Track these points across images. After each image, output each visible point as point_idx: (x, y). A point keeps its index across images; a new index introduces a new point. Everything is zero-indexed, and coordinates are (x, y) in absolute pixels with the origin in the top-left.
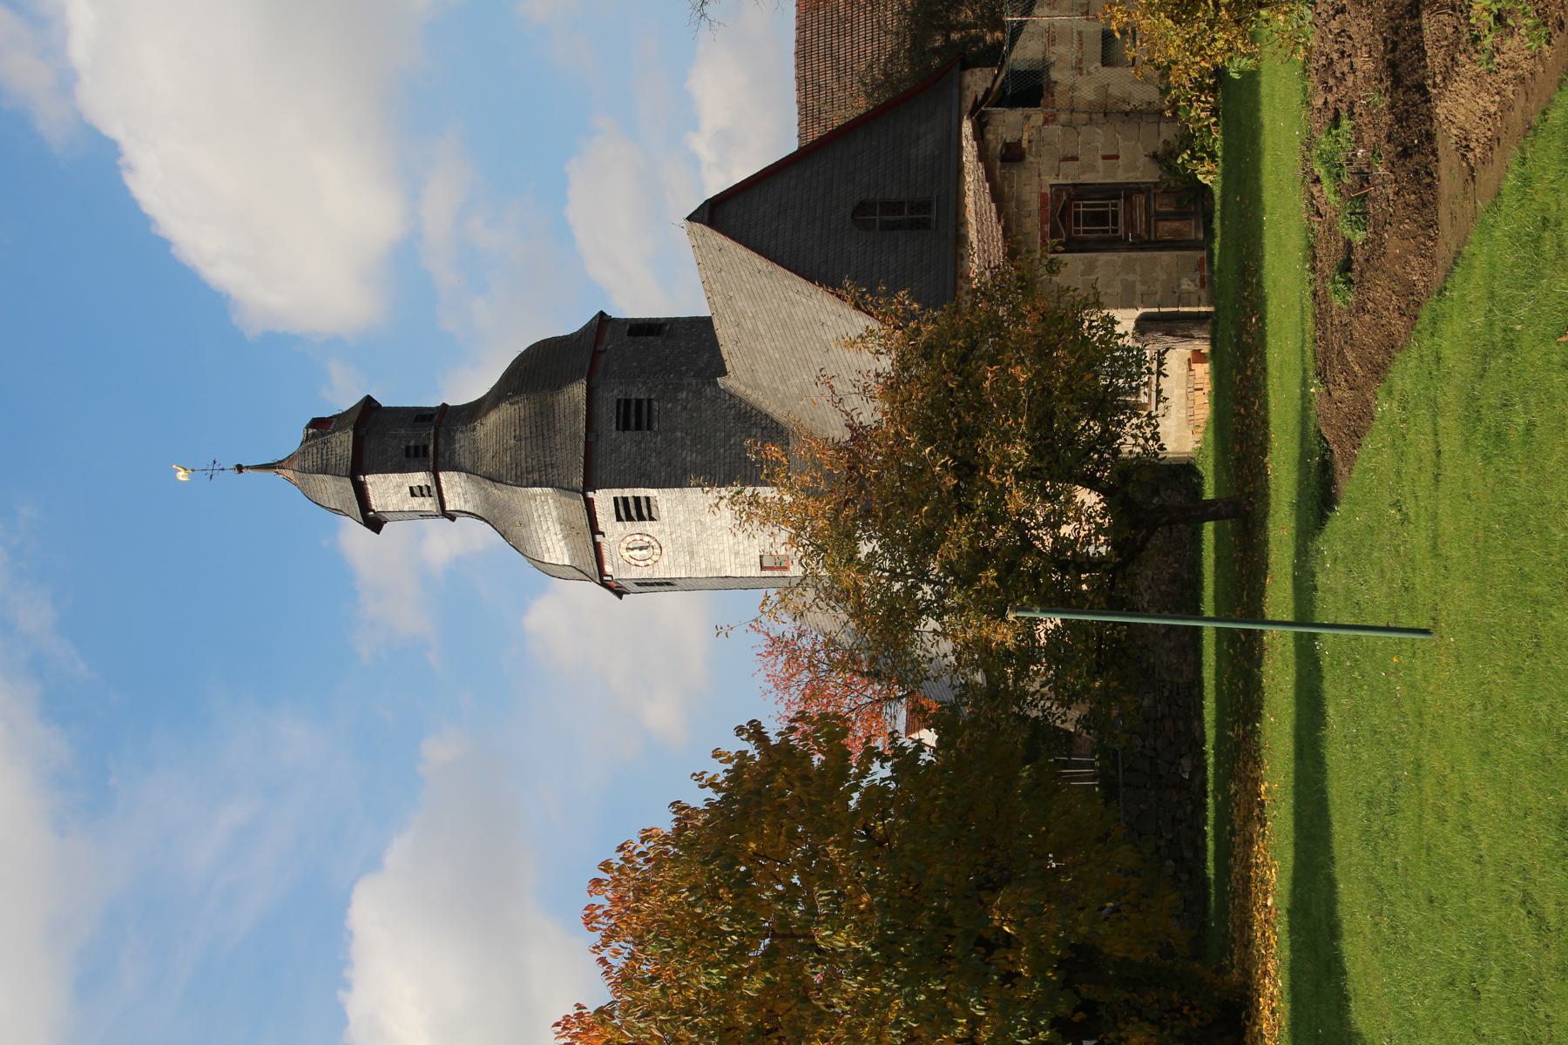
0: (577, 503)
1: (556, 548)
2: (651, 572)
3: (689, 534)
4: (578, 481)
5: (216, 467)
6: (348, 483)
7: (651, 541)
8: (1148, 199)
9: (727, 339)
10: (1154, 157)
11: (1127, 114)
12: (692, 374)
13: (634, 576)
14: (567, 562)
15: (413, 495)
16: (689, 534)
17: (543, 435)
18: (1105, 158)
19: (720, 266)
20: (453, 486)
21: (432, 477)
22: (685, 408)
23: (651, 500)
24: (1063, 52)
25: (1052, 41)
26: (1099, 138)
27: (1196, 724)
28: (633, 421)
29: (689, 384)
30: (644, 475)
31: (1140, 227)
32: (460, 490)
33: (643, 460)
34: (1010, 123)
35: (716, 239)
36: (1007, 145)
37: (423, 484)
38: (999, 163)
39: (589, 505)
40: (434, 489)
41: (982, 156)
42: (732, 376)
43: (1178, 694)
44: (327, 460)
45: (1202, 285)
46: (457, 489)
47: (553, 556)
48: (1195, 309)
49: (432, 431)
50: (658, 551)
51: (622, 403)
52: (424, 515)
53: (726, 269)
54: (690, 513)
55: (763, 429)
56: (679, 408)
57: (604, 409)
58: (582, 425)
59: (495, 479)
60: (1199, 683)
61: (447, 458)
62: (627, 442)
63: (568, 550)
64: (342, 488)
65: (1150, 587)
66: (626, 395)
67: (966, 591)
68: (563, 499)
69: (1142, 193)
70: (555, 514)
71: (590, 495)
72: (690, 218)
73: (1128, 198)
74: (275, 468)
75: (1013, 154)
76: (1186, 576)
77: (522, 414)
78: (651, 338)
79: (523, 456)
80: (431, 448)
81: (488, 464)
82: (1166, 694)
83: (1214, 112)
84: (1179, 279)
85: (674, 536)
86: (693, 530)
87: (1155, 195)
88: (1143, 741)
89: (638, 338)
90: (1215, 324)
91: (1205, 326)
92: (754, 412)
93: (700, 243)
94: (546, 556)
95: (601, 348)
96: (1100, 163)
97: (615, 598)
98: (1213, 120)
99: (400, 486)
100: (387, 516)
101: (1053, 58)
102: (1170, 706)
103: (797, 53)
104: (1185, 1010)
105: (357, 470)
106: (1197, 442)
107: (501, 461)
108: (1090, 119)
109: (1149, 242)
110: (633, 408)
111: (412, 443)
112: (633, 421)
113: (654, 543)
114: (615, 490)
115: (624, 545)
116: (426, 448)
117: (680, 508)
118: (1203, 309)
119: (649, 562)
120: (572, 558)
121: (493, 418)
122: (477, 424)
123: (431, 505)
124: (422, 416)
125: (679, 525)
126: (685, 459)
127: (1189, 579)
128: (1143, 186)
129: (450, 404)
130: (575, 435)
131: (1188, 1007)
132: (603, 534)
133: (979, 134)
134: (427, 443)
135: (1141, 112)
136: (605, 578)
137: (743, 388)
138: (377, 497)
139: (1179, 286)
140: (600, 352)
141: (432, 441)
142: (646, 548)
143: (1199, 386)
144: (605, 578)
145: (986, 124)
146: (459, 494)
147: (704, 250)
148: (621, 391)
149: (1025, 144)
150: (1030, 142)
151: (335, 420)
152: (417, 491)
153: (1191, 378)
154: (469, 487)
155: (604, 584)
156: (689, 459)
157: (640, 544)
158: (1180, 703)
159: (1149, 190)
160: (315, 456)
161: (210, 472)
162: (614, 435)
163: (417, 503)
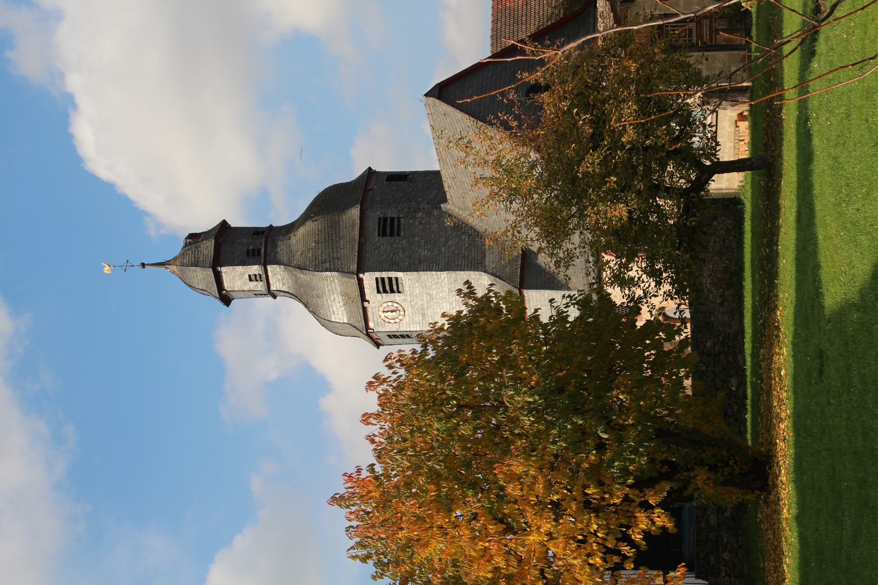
1: (339, 313)
2: (397, 327)
3: (422, 302)
4: (354, 267)
5: (128, 264)
6: (210, 272)
7: (399, 306)
9: (448, 176)
12: (425, 202)
13: (387, 330)
14: (346, 321)
15: (251, 280)
16: (422, 302)
17: (332, 240)
19: (444, 126)
20: (275, 274)
21: (263, 268)
22: (421, 223)
23: (399, 281)
27: (740, 357)
28: (388, 231)
29: (423, 208)
30: (395, 263)
31: (706, 38)
32: (280, 277)
33: (394, 254)
35: (443, 107)
37: (257, 273)
39: (360, 282)
40: (264, 276)
42: (450, 203)
43: (728, 339)
44: (198, 258)
46: (278, 276)
47: (337, 317)
49: (264, 240)
50: (402, 313)
51: (382, 219)
52: (258, 294)
53: (448, 127)
54: (423, 288)
55: (469, 236)
56: (417, 223)
57: (371, 223)
58: (357, 232)
59: (301, 268)
60: (742, 331)
61: (272, 257)
62: (385, 244)
63: (347, 313)
64: (207, 275)
65: (711, 275)
66: (384, 215)
68: (346, 279)
69: (708, 18)
70: (338, 289)
71: (361, 275)
72: (426, 95)
74: (165, 265)
76: (734, 268)
77: (320, 228)
78: (400, 182)
79: (320, 253)
80: (263, 251)
81: (298, 259)
82: (721, 339)
85: (413, 303)
86: (425, 300)
87: (715, 19)
88: (707, 367)
89: (392, 183)
90: (752, 91)
91: (746, 95)
92: (464, 225)
93: (433, 112)
94: (333, 317)
95: (370, 188)
97: (375, 348)
99: (242, 274)
100: (234, 294)
102: (723, 346)
103: (492, 37)
104: (731, 463)
105: (217, 263)
106: (741, 182)
107: (306, 256)
109: (712, 46)
110: (388, 223)
111: (251, 248)
112: (388, 231)
113: (400, 308)
115: (381, 309)
116: (259, 250)
117: (417, 285)
119: (397, 320)
120: (349, 318)
121: (302, 231)
122: (292, 235)
123: (261, 286)
124: (256, 232)
125: (416, 296)
126: (420, 254)
127: (735, 270)
128: (707, 14)
129: (274, 225)
130: (353, 239)
131: (732, 461)
134: (260, 247)
136: (369, 331)
137: (457, 210)
138: (228, 281)
140: (369, 190)
141: (263, 246)
142: (395, 311)
143: (742, 138)
144: (369, 331)
146: (279, 280)
147: (434, 116)
148: (381, 213)
151: (203, 234)
152: (253, 278)
153: (737, 132)
154: (286, 275)
155: (368, 335)
156: (423, 254)
157: (392, 308)
158: (730, 344)
159: (712, 16)
160: (190, 255)
161: (124, 268)
163: (253, 285)
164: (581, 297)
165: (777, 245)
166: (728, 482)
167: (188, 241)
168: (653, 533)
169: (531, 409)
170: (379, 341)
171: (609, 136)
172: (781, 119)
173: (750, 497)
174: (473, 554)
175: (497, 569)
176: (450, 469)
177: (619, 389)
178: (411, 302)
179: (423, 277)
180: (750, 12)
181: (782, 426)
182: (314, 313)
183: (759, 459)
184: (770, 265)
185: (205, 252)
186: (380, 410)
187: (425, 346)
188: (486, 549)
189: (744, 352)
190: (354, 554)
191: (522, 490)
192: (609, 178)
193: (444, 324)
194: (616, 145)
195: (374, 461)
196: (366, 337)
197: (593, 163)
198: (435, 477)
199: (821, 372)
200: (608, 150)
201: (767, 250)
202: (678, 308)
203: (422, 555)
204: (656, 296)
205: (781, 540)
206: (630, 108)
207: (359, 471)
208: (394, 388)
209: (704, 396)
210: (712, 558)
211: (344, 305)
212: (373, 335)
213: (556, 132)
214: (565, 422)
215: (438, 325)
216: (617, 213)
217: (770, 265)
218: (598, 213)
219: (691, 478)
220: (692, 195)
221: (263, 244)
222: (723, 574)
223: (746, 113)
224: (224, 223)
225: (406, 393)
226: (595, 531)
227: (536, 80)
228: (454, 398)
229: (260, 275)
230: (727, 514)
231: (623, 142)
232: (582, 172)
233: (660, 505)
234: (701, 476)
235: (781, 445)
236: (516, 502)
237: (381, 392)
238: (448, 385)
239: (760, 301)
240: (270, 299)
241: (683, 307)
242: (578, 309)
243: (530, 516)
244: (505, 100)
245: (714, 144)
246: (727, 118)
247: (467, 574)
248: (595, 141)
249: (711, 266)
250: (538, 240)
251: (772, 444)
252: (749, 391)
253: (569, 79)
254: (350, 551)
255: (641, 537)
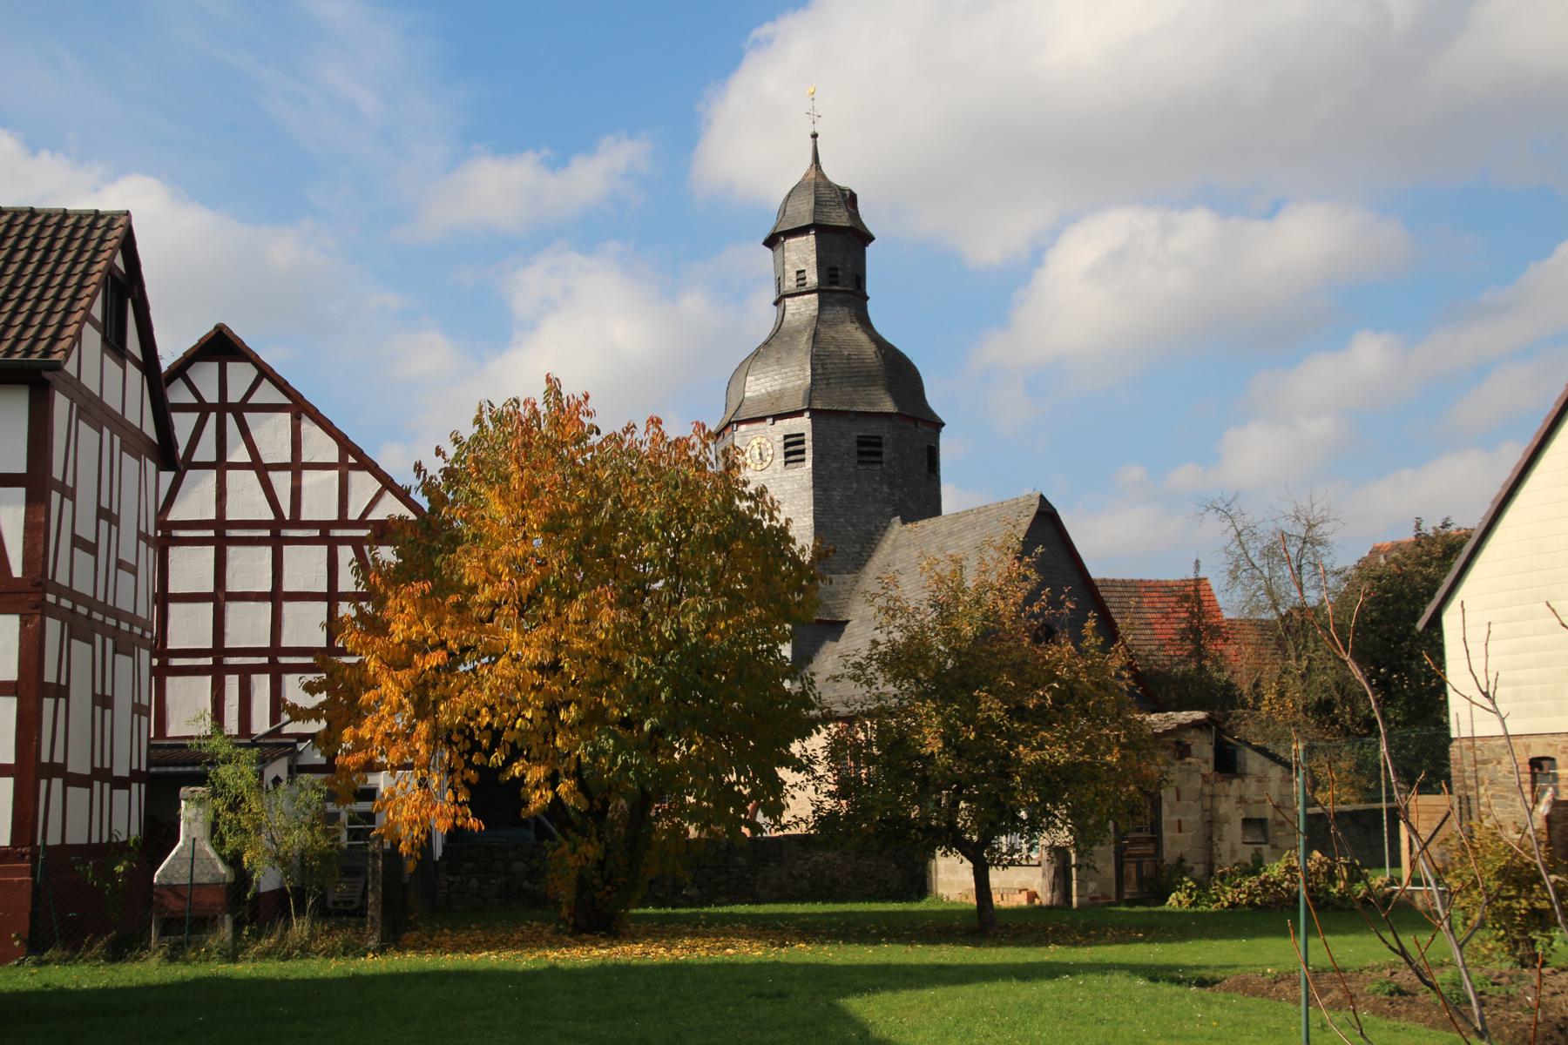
0: (800, 403)
1: (758, 386)
4: (818, 405)
6: (808, 221)
8: (1150, 855)
10: (1181, 860)
11: (1210, 838)
15: (798, 272)
18: (1180, 821)
23: (800, 464)
24: (1251, 788)
25: (1260, 780)
26: (1193, 818)
27: (725, 900)
28: (865, 449)
33: (835, 456)
34: (1203, 748)
36: (1188, 747)
37: (807, 280)
38: (1174, 740)
39: (799, 413)
41: (1182, 727)
45: (1092, 899)
46: (804, 308)
47: (753, 383)
48: (1074, 893)
49: (850, 289)
50: (759, 467)
52: (779, 282)
55: (860, 554)
56: (875, 486)
58: (862, 409)
59: (816, 339)
60: (757, 901)
61: (829, 300)
62: (848, 444)
67: (955, 715)
68: (801, 395)
70: (789, 385)
71: (807, 414)
72: (1042, 497)
73: (1152, 840)
75: (1183, 751)
78: (926, 464)
80: (836, 288)
82: (747, 876)
83: (1233, 905)
84: (1095, 880)
95: (919, 424)
96: (1175, 818)
98: (1226, 904)
99: (806, 262)
100: (779, 251)
101: (1247, 781)
104: (609, 888)
105: (822, 230)
106: (948, 898)
108: (1206, 810)
111: (840, 273)
112: (865, 449)
113: (765, 465)
114: (810, 434)
116: (836, 283)
117: (796, 486)
118: (1075, 900)
121: (862, 337)
122: (857, 325)
124: (859, 280)
130: (853, 403)
132: (773, 424)
133: (1196, 725)
135: (1211, 850)
137: (892, 537)
139: (1091, 880)
140: (916, 424)
145: (1201, 729)
149: (1188, 760)
150: (1189, 764)
152: (801, 275)
155: (730, 424)
157: (764, 455)
162: (854, 434)
163: (791, 276)
164: (812, 698)
165: (888, 942)
166: (582, 884)
167: (848, 193)
168: (523, 789)
169: (681, 634)
170: (721, 438)
171: (1024, 730)
172: (1047, 945)
173: (565, 912)
174: (493, 561)
175: (473, 589)
176: (598, 530)
177: (704, 745)
178: (773, 479)
179: (804, 493)
180: (1164, 904)
181: (661, 950)
182: (757, 354)
183: (614, 923)
184: (855, 934)
185: (834, 214)
186: (668, 440)
187: (751, 497)
188: (499, 576)
189: (733, 904)
190: (483, 409)
191: (576, 622)
192: (974, 730)
193: (778, 521)
194: (1014, 738)
195: (604, 433)
196: (726, 421)
197: (990, 709)
198: (588, 510)
199: (760, 995)
200: (1007, 728)
201: (874, 931)
202: (802, 819)
203: (490, 495)
204: (816, 790)
205: (517, 949)
206: (1060, 755)
207: (589, 414)
208: (697, 457)
209: (687, 852)
210: (471, 865)
211: (768, 393)
212: (729, 430)
213: (1025, 662)
214: (664, 676)
215: (776, 513)
216: (929, 739)
217: (855, 934)
218: (929, 717)
219: (589, 837)
220: (950, 835)
221: (845, 288)
222: (451, 879)
223: (1037, 902)
224: (871, 238)
225: (691, 473)
226: (524, 716)
227: (1086, 637)
228: (689, 534)
229: (804, 285)
230: (526, 884)
231: (1017, 747)
232: (979, 696)
233: (557, 798)
234: (592, 850)
235: (638, 949)
236: (558, 614)
237: (691, 442)
238: (706, 527)
239: (806, 923)
240: (773, 297)
241: (804, 825)
242: (797, 693)
243: (546, 632)
244: (1063, 596)
245: (1005, 862)
246: (1031, 878)
247: (468, 552)
248: (1018, 712)
249: (838, 862)
250: (889, 641)
251: (634, 939)
252: (683, 911)
253: (1092, 678)
254: (487, 404)
255: (517, 774)
